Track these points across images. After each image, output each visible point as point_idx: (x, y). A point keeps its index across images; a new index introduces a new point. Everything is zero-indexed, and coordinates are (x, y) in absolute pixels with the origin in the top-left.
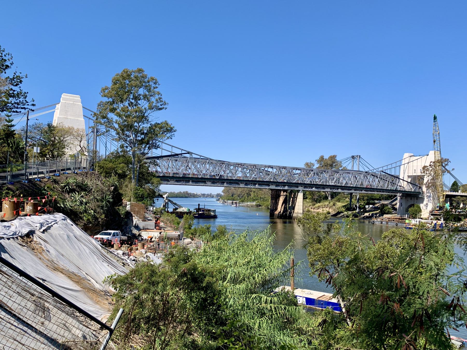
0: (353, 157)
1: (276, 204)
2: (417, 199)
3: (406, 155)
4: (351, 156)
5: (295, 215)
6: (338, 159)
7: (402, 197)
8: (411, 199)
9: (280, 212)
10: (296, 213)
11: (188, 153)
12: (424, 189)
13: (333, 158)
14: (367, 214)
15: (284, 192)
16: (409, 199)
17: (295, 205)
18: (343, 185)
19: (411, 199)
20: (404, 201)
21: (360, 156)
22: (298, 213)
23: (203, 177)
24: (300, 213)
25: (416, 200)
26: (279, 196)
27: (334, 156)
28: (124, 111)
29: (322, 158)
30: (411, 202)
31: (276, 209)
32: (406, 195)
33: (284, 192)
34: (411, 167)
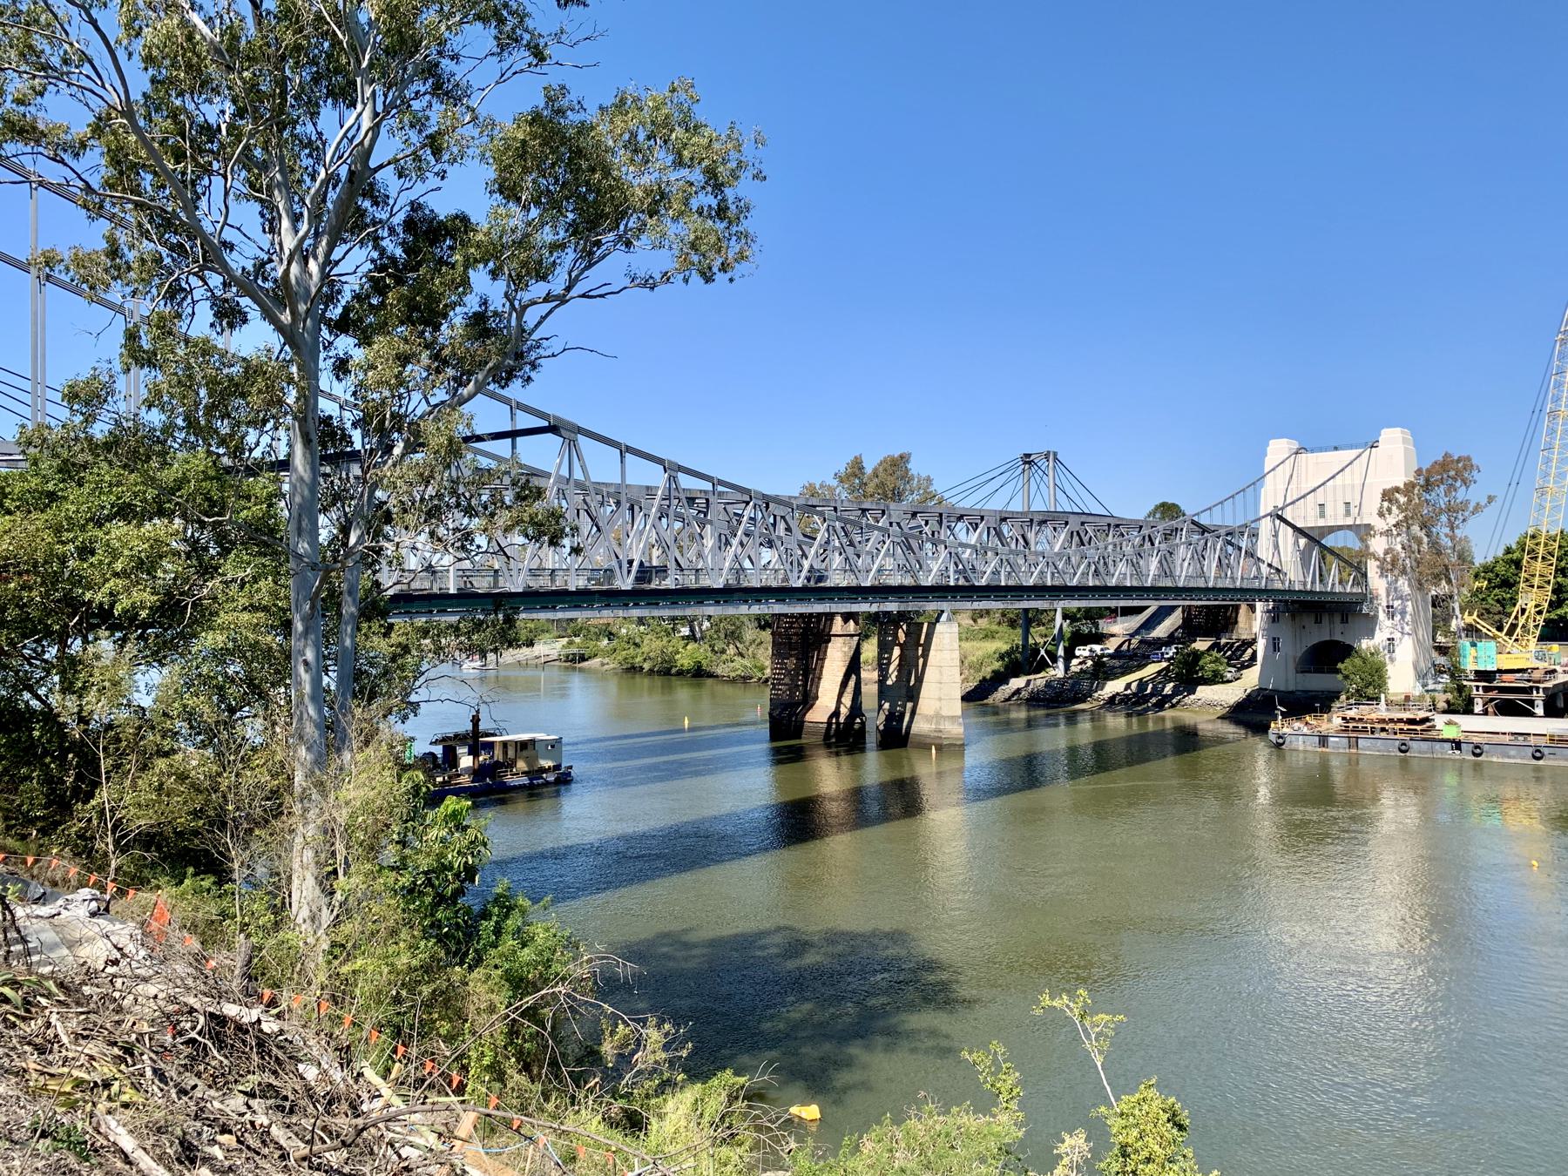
0: (1027, 460)
1: (808, 674)
2: (1344, 620)
3: (1278, 448)
4: (1019, 454)
5: (920, 727)
6: (914, 467)
7: (1274, 617)
8: (1318, 621)
9: (836, 713)
10: (928, 719)
11: (553, 429)
12: (1377, 583)
13: (898, 465)
14: (1115, 687)
15: (846, 620)
16: (1308, 621)
17: (920, 680)
18: (1149, 584)
19: (1318, 621)
20: (1285, 631)
21: (1055, 454)
22: (938, 717)
23: (535, 584)
24: (953, 718)
25: (1338, 627)
26: (824, 638)
27: (901, 457)
28: (278, 774)
29: (857, 466)
30: (1319, 634)
31: (809, 700)
32: (1295, 608)
33: (846, 620)
34: (1327, 487)
